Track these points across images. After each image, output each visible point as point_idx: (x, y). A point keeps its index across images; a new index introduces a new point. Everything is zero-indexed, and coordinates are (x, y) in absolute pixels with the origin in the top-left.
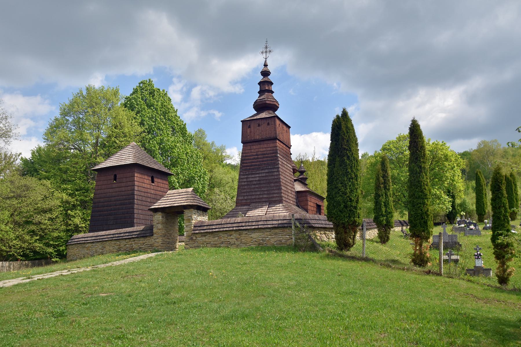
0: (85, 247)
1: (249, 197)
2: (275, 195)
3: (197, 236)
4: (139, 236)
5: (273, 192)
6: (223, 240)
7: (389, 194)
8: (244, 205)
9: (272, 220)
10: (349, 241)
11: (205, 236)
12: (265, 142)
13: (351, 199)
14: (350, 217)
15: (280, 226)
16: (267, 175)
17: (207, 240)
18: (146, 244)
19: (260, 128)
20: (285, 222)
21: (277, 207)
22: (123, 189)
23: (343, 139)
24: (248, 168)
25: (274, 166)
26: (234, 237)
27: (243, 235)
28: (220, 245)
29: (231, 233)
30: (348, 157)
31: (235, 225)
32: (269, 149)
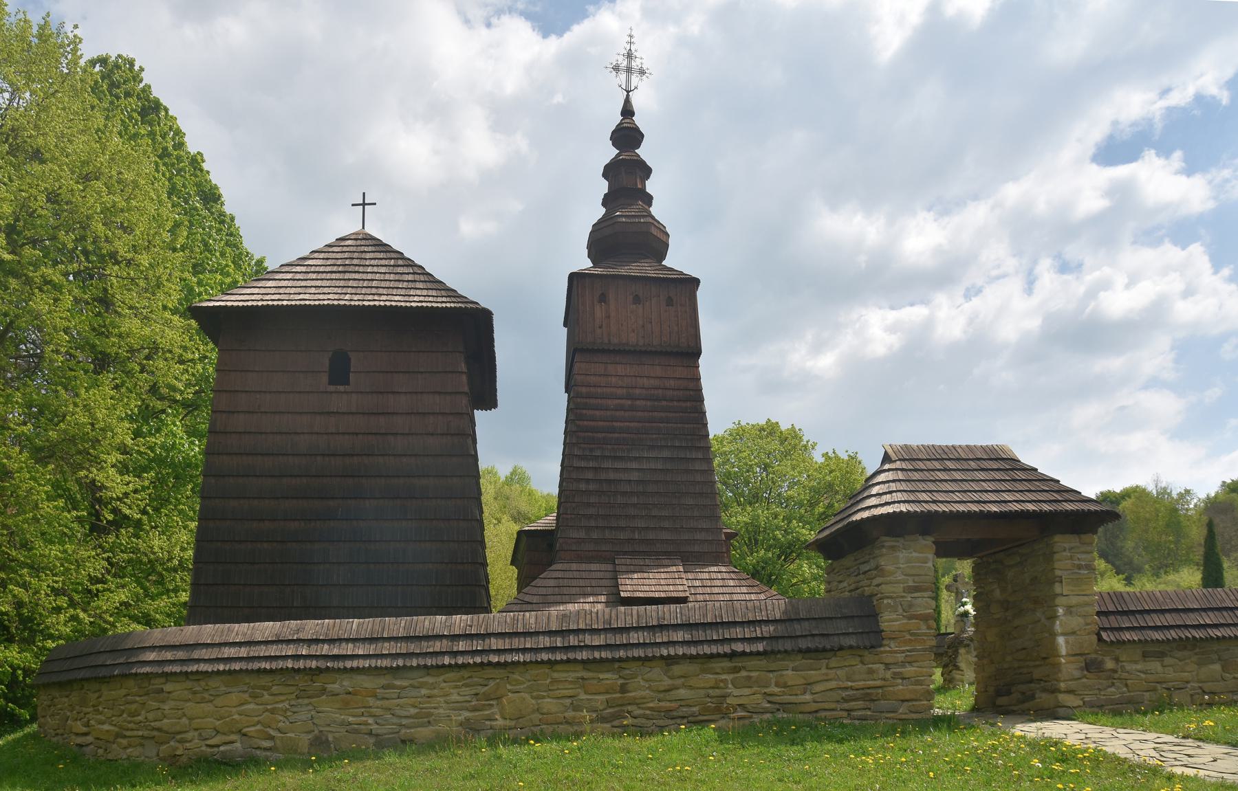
1: (608, 535)
2: (698, 536)
8: (590, 560)
11: (1161, 655)
18: (833, 684)
21: (714, 576)
24: (600, 435)
32: (672, 382)
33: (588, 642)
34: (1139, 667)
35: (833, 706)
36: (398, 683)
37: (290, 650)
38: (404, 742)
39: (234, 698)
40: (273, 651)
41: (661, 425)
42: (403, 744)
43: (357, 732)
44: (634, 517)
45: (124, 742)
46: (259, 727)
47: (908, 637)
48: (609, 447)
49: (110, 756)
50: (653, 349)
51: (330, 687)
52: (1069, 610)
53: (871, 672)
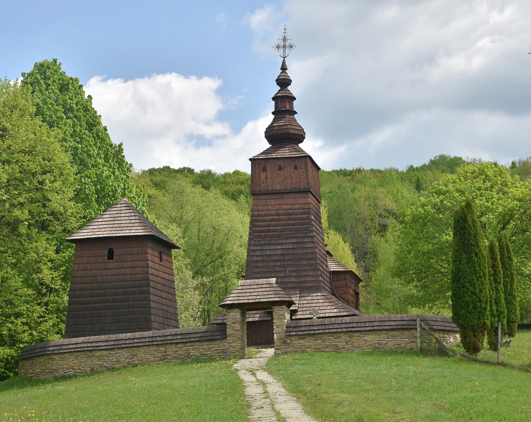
0: (94, 356)
2: (309, 279)
3: (292, 338)
4: (204, 339)
5: (306, 273)
6: (329, 344)
7: (500, 288)
9: (389, 321)
10: (479, 345)
11: (304, 339)
12: (290, 195)
13: (480, 300)
14: (479, 319)
15: (399, 327)
16: (295, 246)
17: (306, 344)
18: (215, 349)
19: (282, 173)
20: (404, 323)
21: (314, 298)
22: (128, 271)
23: (470, 234)
24: (263, 234)
25: (306, 233)
26: (342, 340)
27: (355, 338)
28: (324, 349)
29: (338, 335)
30: (476, 254)
31: (343, 326)
32: (297, 206)
33: (157, 340)
34: (297, 342)
35: (215, 354)
36: (112, 352)
37: (86, 345)
38: (114, 368)
39: (71, 359)
40: (82, 345)
41: (292, 227)
42: (112, 369)
43: (102, 366)
44: (278, 272)
45: (43, 374)
46: (77, 367)
48: (267, 239)
49: (39, 379)
50: (288, 191)
52: (277, 327)
53: (224, 345)
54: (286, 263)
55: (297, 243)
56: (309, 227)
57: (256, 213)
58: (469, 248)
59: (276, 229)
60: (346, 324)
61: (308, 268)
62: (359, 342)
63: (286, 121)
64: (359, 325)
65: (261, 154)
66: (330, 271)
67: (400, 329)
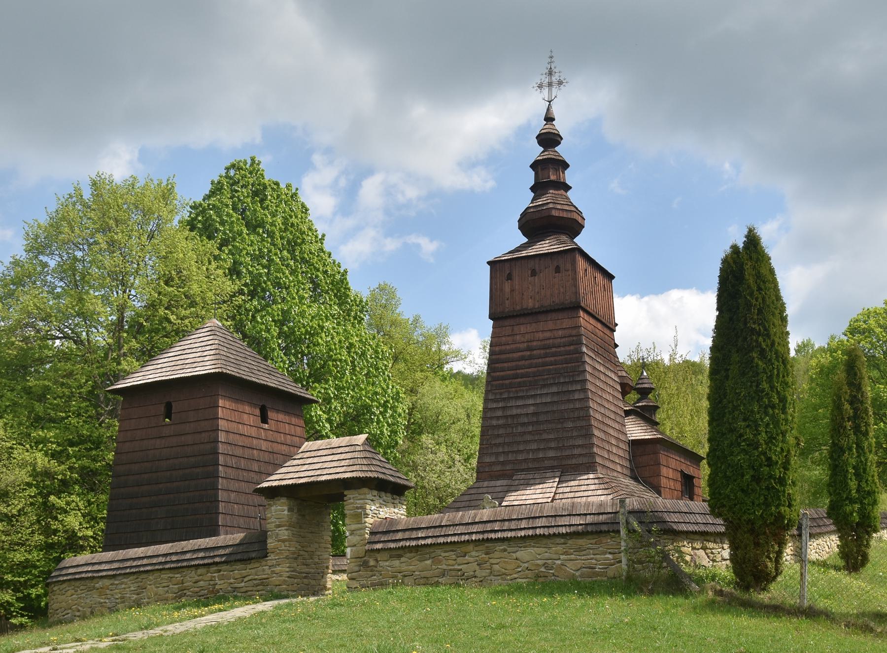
1: (511, 457)
2: (576, 451)
4: (233, 558)
5: (571, 442)
6: (444, 567)
7: (866, 445)
8: (498, 478)
10: (766, 567)
11: (399, 557)
13: (769, 459)
14: (767, 505)
15: (589, 529)
16: (555, 399)
17: (404, 567)
18: (250, 577)
21: (582, 482)
23: (749, 306)
24: (507, 382)
25: (573, 376)
26: (472, 559)
27: (497, 554)
28: (436, 579)
29: (464, 549)
30: (762, 353)
31: (475, 528)
32: (560, 333)
34: (387, 564)
41: (551, 367)
47: (278, 552)
48: (513, 389)
51: (97, 585)
53: (264, 570)
54: (541, 427)
55: (558, 393)
56: (578, 366)
57: (497, 349)
58: (745, 339)
59: (527, 372)
60: (480, 525)
61: (575, 434)
62: (505, 562)
63: (548, 198)
64: (506, 525)
65: (510, 252)
66: (629, 440)
67: (592, 533)
